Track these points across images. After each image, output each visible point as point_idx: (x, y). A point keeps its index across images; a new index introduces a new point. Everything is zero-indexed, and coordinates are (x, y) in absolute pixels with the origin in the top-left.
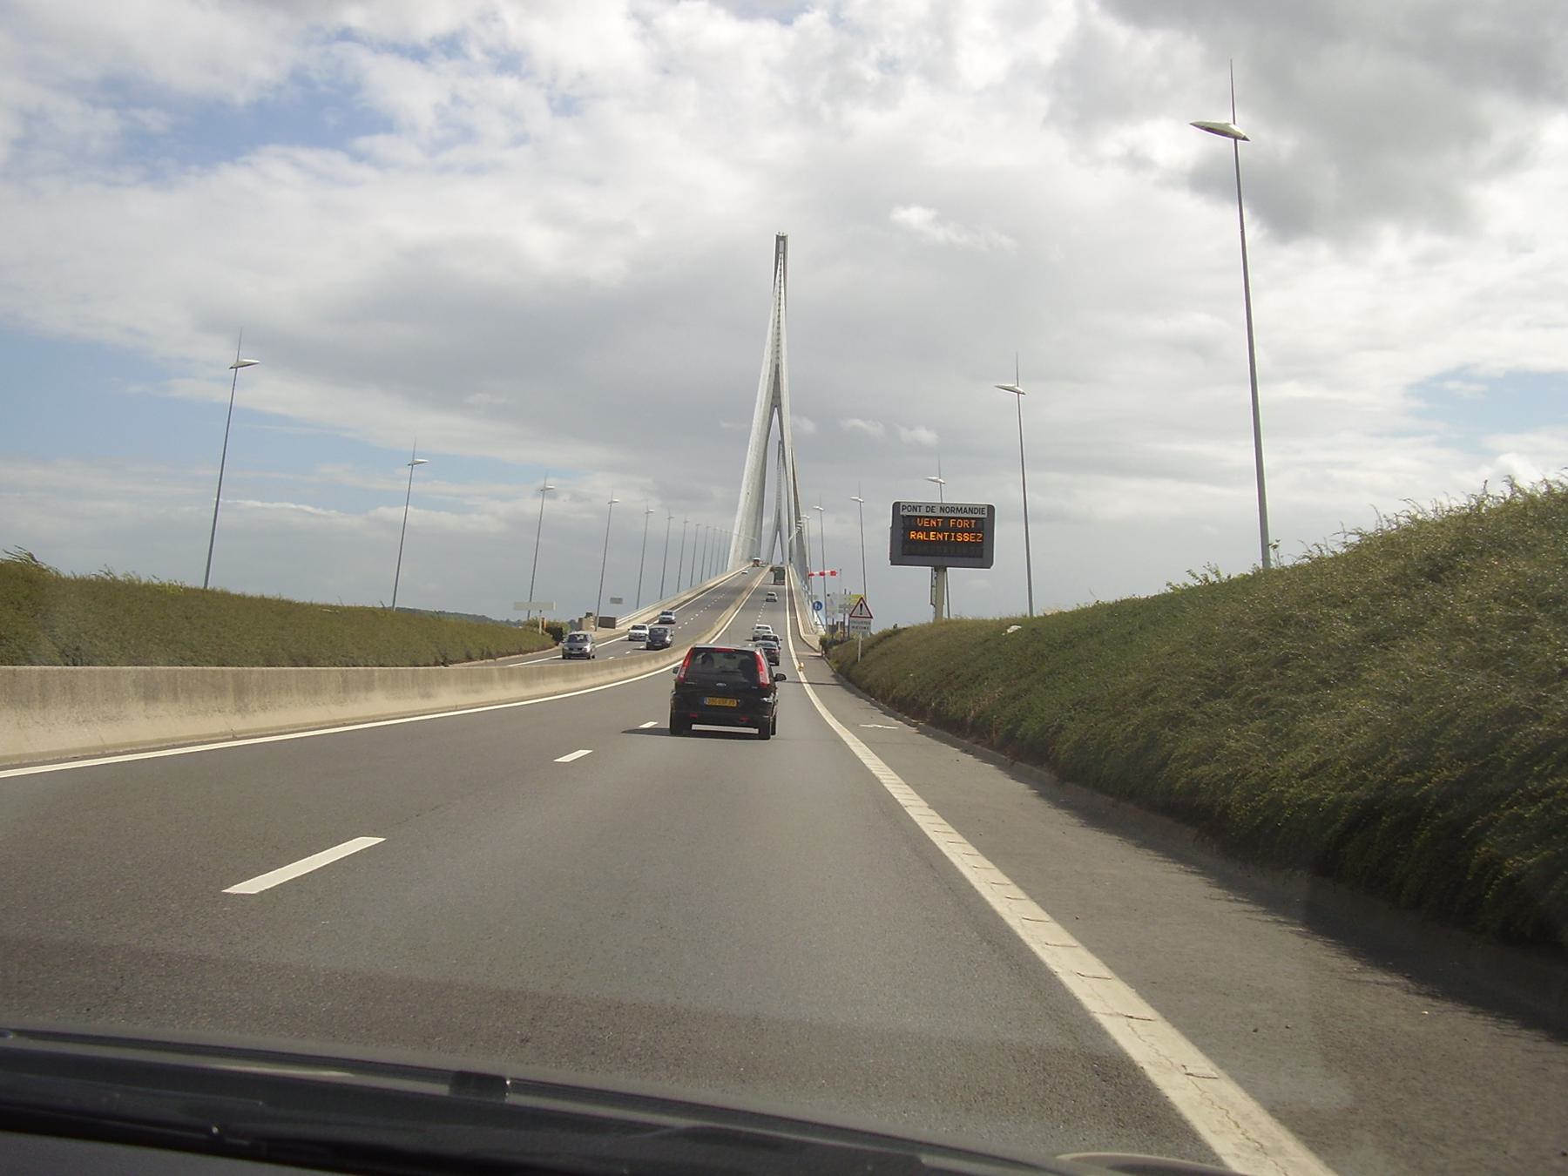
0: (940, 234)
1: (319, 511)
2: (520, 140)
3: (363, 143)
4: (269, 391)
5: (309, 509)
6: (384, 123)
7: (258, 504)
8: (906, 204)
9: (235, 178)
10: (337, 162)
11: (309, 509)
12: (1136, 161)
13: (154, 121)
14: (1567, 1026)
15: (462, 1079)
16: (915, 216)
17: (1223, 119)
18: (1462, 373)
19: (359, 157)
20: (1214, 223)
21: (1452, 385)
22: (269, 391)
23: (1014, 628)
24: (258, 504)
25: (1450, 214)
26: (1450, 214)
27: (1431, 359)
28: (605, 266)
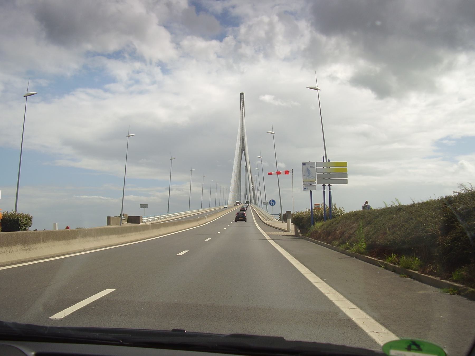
0: (277, 103)
1: (106, 198)
2: (154, 83)
3: (107, 86)
4: (88, 163)
5: (102, 197)
6: (113, 80)
7: (87, 197)
8: (264, 95)
9: (69, 99)
10: (100, 92)
11: (102, 197)
12: (333, 78)
13: (43, 83)
14: (474, 297)
15: (174, 330)
16: (267, 98)
17: (314, 86)
18: (448, 138)
19: (106, 91)
20: (366, 95)
21: (445, 142)
22: (88, 163)
23: (318, 224)
24: (87, 197)
25: (431, 88)
26: (431, 88)
27: (439, 134)
28: (182, 119)
